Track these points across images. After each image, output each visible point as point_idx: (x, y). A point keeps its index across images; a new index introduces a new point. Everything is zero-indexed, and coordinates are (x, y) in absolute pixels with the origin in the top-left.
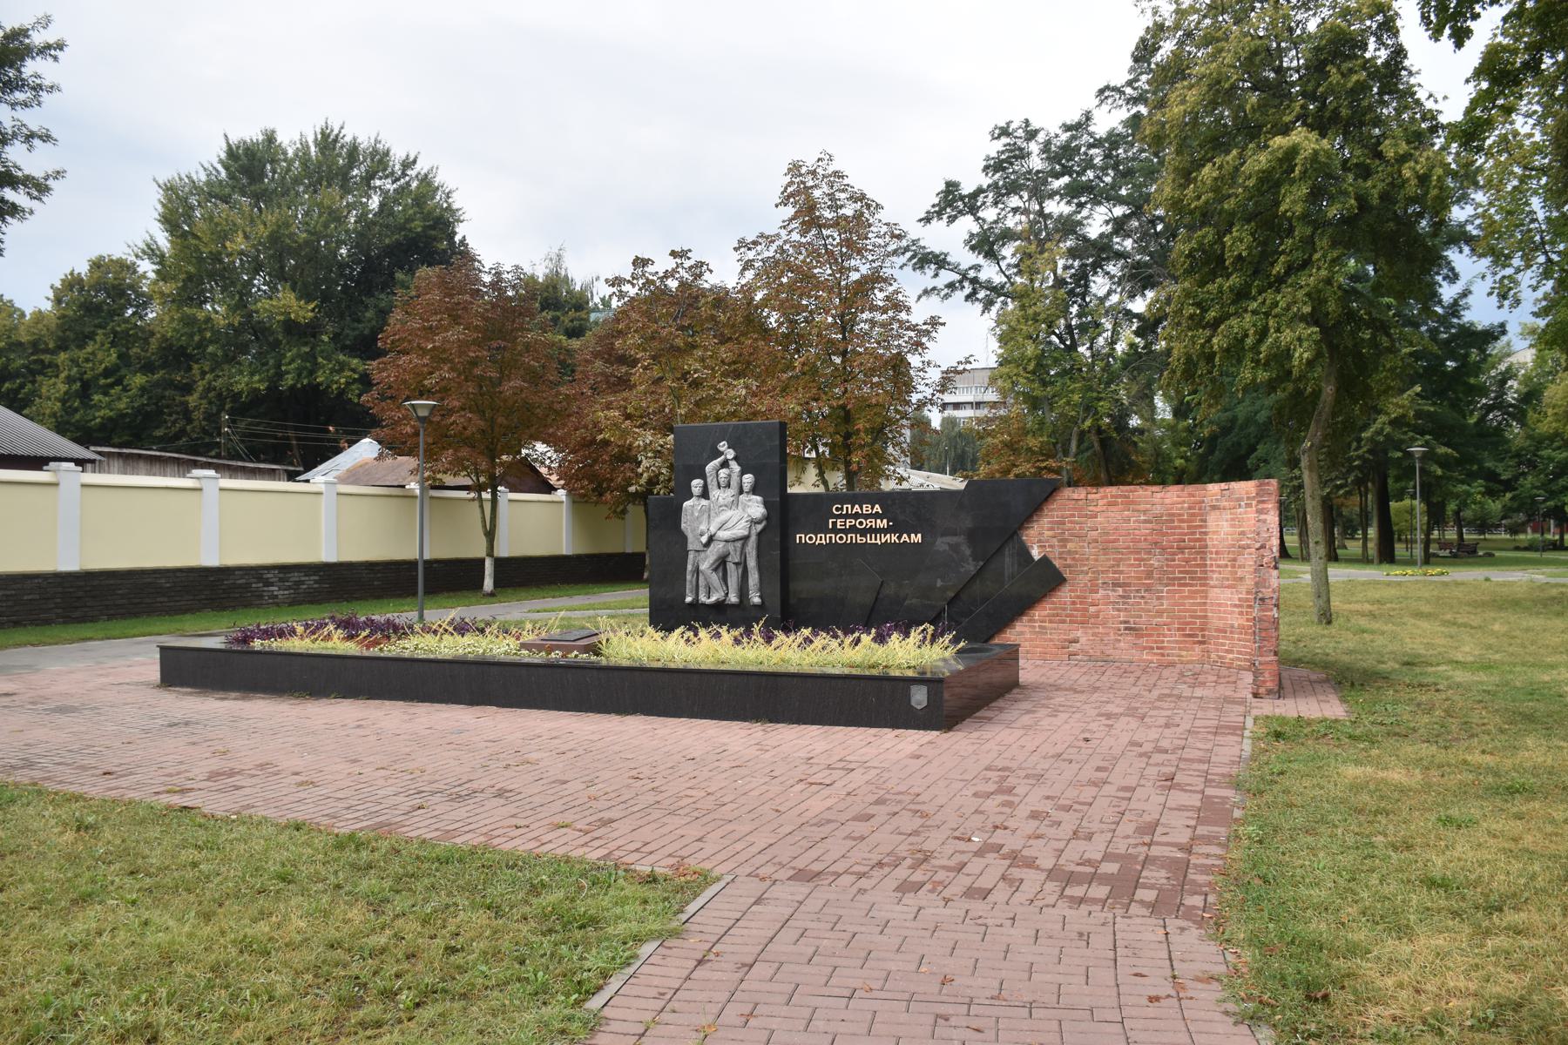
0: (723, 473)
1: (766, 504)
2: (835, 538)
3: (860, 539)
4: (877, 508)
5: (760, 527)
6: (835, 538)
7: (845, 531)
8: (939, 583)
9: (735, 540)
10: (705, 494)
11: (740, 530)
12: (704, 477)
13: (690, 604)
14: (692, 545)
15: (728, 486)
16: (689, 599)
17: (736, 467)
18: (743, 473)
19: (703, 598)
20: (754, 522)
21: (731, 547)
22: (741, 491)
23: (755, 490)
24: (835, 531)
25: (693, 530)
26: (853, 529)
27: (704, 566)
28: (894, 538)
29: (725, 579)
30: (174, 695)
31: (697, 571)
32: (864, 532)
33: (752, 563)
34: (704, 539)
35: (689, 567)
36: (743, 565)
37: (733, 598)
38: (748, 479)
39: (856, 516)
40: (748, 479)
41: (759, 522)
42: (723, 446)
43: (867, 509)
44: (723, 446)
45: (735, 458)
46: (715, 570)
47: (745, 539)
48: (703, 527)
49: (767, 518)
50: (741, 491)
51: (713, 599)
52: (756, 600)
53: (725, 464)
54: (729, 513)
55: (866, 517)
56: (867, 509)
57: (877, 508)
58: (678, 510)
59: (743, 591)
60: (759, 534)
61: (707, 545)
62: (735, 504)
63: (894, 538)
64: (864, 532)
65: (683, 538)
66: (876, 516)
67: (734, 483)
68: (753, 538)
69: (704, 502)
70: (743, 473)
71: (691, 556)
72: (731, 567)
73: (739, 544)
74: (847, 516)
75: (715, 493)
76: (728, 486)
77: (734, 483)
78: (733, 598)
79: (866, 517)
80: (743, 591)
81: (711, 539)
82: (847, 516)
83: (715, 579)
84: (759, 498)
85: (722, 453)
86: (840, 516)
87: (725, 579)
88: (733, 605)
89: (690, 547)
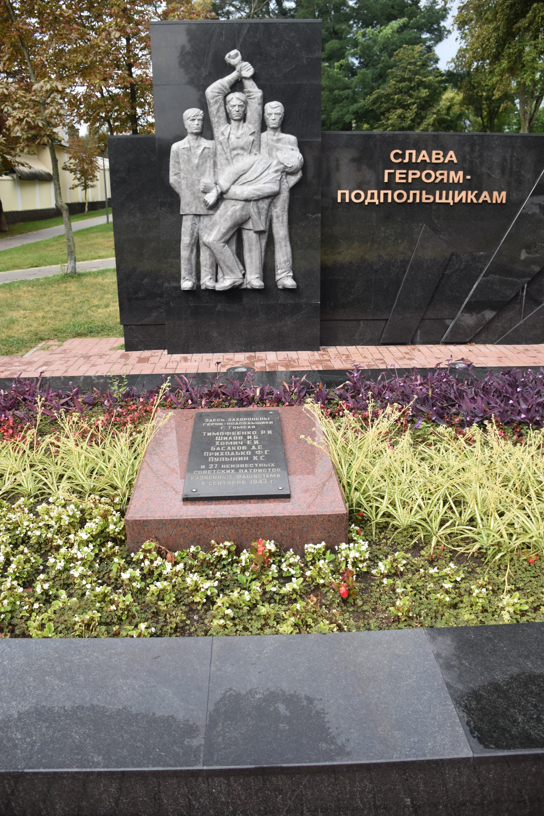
0: (235, 98)
1: (301, 146)
2: (392, 196)
3: (426, 198)
4: (452, 156)
5: (293, 180)
6: (392, 196)
7: (407, 187)
8: (524, 255)
9: (259, 199)
10: (206, 131)
11: (267, 185)
12: (203, 105)
13: (187, 292)
14: (187, 205)
15: (243, 118)
16: (186, 284)
17: (256, 92)
18: (265, 100)
19: (207, 282)
20: (287, 172)
21: (252, 208)
22: (264, 127)
23: (285, 126)
24: (391, 185)
25: (191, 185)
26: (418, 184)
27: (87, 294)
28: (471, 197)
29: (240, 254)
30: (265, 192)
31: (197, 244)
32: (431, 188)
33: (281, 231)
34: (211, 198)
35: (185, 239)
36: (268, 236)
37: (254, 280)
38: (275, 109)
39: (422, 166)
40: (275, 109)
41: (293, 173)
42: (233, 56)
43: (437, 156)
44: (233, 56)
45: (254, 77)
46: (227, 242)
47: (273, 197)
48: (207, 180)
49: (304, 167)
50: (264, 127)
51: (225, 283)
52: (290, 283)
53: (237, 86)
54: (243, 161)
55: (436, 167)
56: (437, 156)
57: (452, 156)
58: (164, 153)
59: (268, 270)
60: (293, 190)
61: (215, 207)
62: (255, 146)
63: (471, 197)
64: (431, 188)
65: (172, 199)
66: (450, 166)
67: (253, 113)
68: (285, 195)
69: (205, 143)
70: (265, 100)
71: (187, 224)
72: (250, 237)
73: (264, 205)
74: (410, 166)
75: (221, 130)
76: (243, 118)
77: (253, 113)
78: (254, 280)
79: (436, 167)
80: (268, 270)
81: (221, 197)
82: (410, 166)
83: (227, 254)
84: (292, 138)
85: (232, 68)
86: (401, 166)
87: (240, 254)
88: (254, 290)
89: (184, 208)
